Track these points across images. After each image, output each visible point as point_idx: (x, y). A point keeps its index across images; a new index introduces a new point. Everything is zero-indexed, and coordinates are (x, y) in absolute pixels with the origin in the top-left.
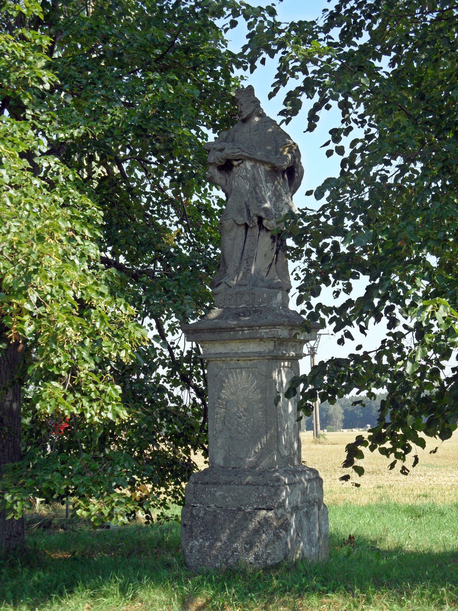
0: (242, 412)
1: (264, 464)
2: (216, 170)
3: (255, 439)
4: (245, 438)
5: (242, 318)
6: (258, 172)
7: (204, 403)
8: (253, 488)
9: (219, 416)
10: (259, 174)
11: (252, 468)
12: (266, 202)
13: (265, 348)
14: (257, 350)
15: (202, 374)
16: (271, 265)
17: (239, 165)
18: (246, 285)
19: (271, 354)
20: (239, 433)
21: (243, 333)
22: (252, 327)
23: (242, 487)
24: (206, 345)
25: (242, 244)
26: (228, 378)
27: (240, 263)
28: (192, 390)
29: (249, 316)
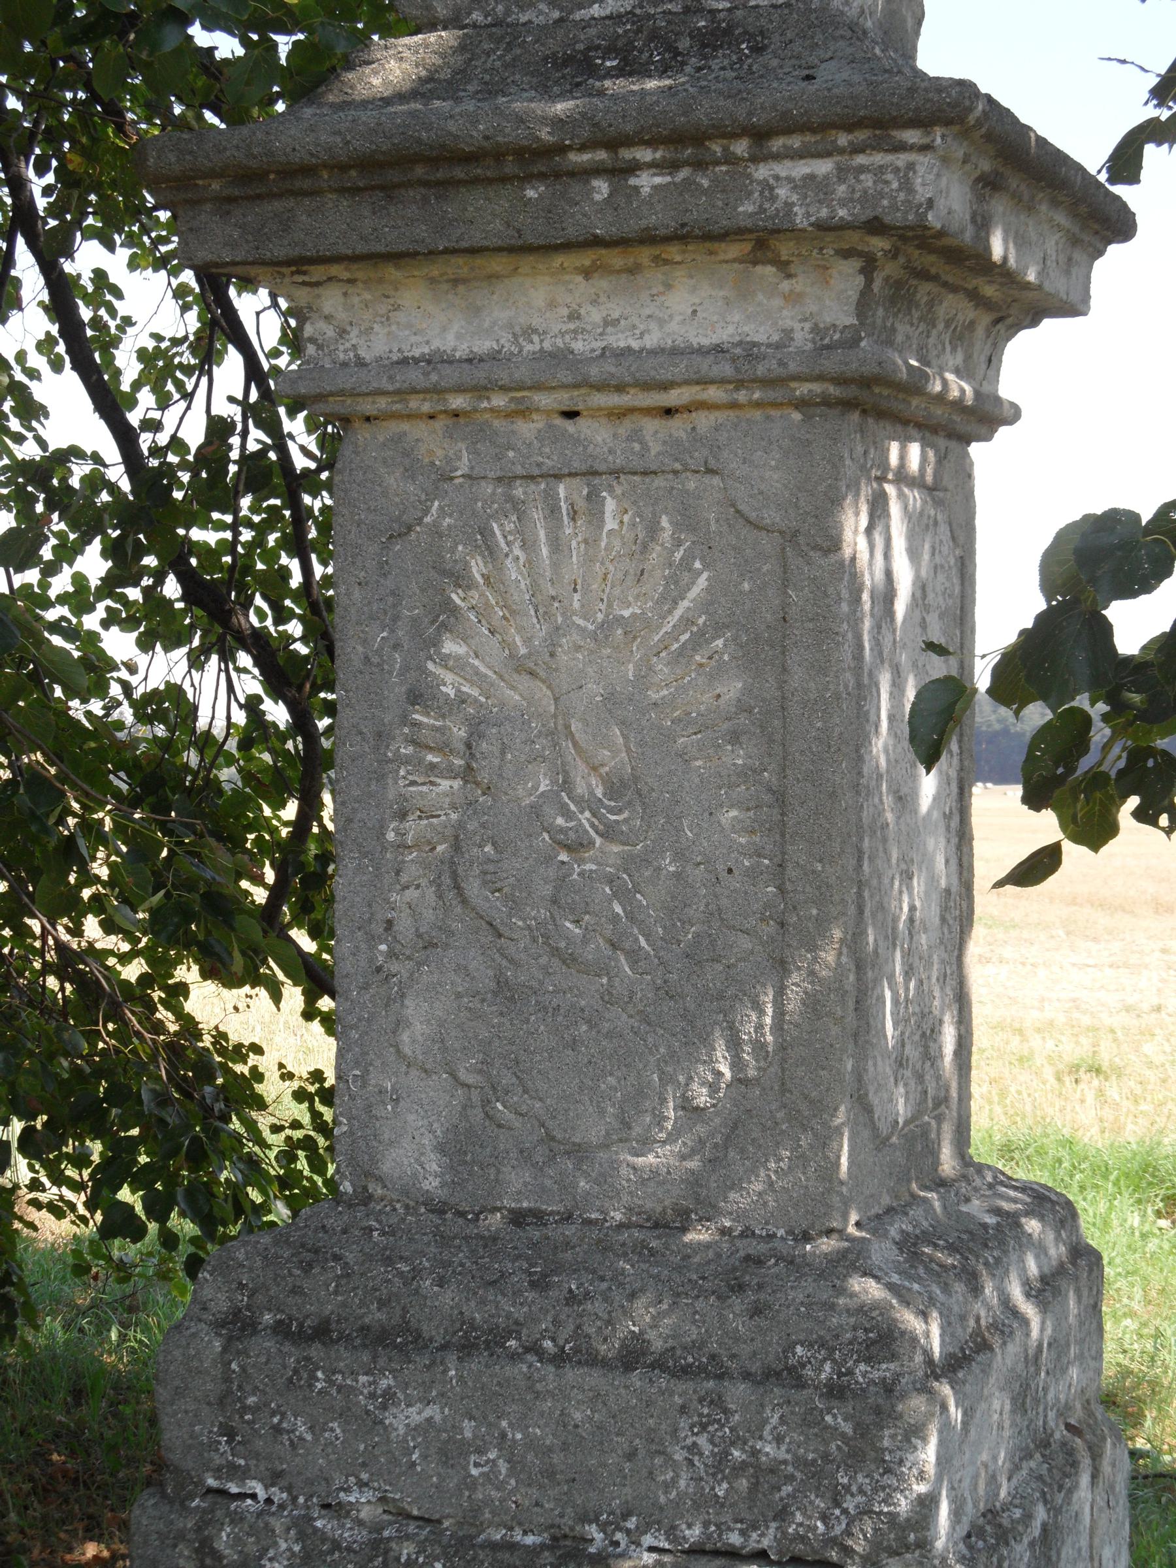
0: (591, 804)
1: (752, 1195)
3: (692, 1005)
4: (608, 998)
7: (302, 723)
8: (682, 1391)
9: (413, 827)
11: (658, 1225)
13: (788, 318)
14: (723, 334)
15: (296, 580)
19: (831, 364)
20: (570, 960)
21: (623, 194)
22: (698, 138)
23: (594, 1378)
24: (331, 300)
26: (490, 551)
28: (244, 659)
29: (663, 72)
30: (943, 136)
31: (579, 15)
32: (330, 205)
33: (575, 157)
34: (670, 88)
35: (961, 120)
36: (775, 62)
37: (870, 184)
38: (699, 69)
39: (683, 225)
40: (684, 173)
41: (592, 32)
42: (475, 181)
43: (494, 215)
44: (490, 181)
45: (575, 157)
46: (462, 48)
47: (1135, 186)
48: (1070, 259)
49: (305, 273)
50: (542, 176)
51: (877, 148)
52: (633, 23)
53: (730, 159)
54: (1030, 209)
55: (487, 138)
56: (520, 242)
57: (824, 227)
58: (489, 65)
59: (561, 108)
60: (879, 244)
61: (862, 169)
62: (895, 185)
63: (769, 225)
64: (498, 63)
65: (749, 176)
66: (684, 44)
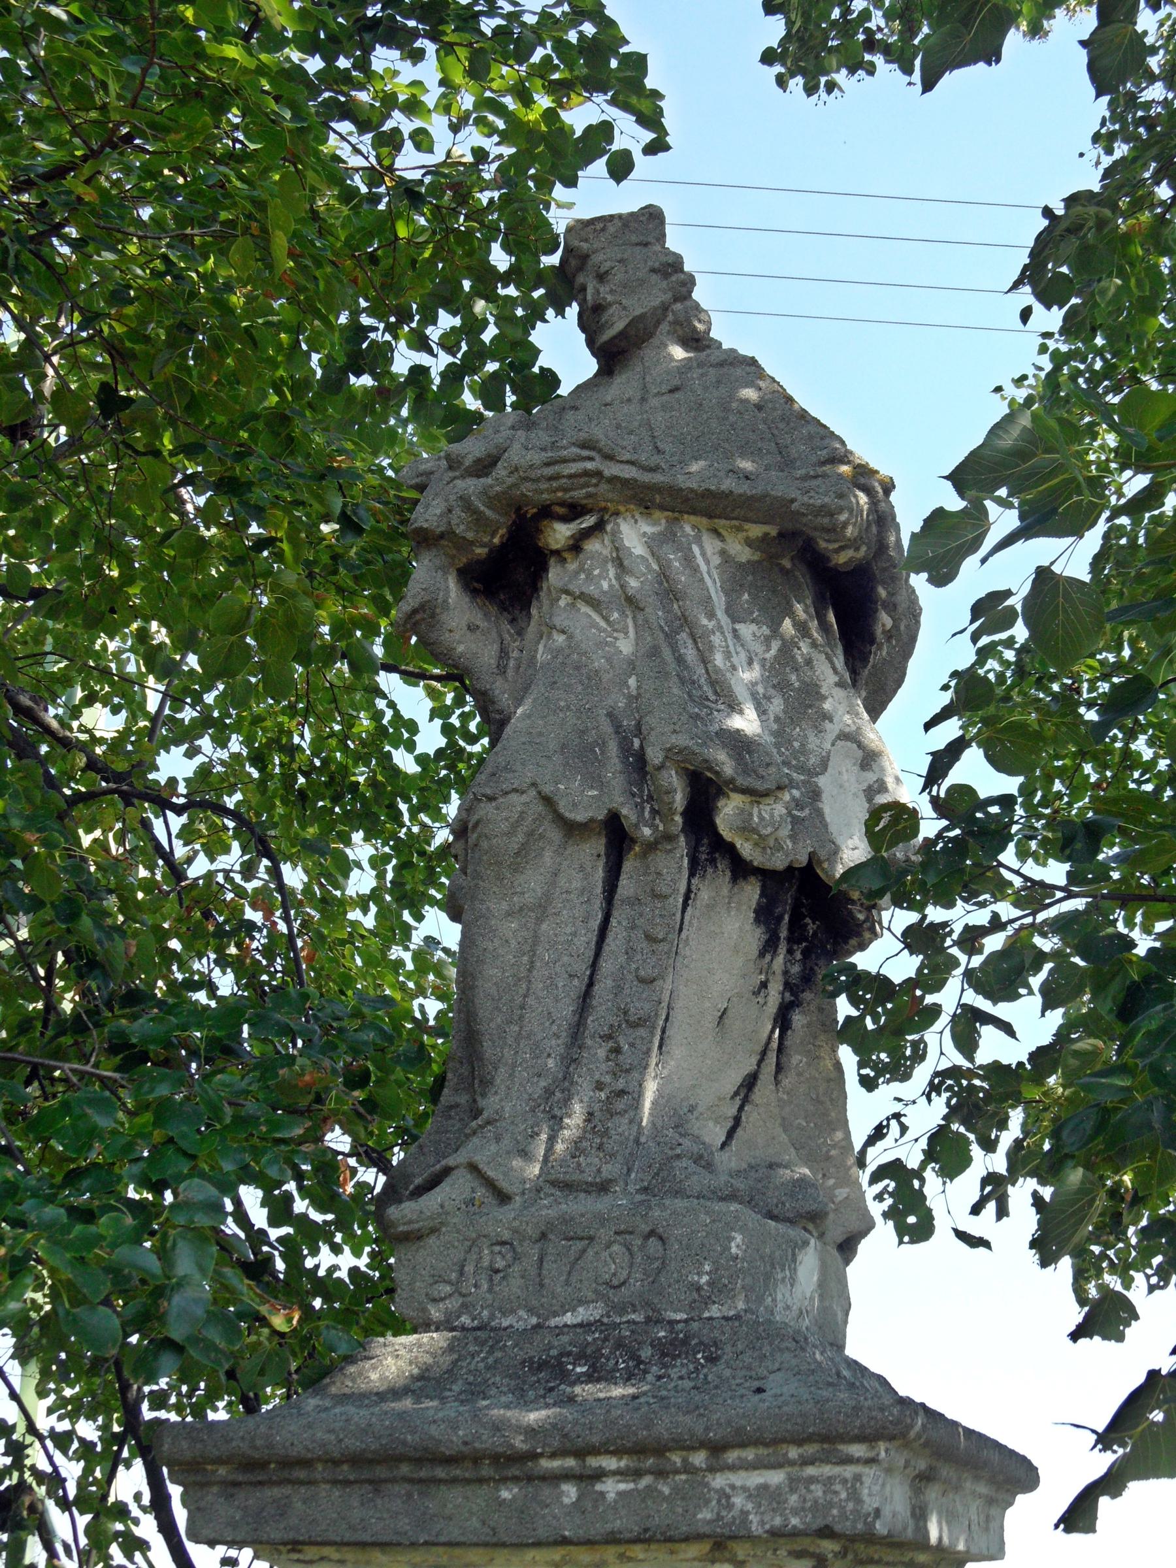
2: (452, 583)
5: (584, 1391)
6: (689, 560)
10: (696, 570)
12: (734, 707)
16: (750, 1082)
17: (576, 546)
18: (603, 1187)
22: (660, 1450)
25: (586, 939)
27: (570, 1061)
29: (628, 1378)
30: (887, 1451)
31: (553, 1322)
32: (324, 1494)
33: (546, 1464)
34: (635, 1397)
35: (904, 1435)
36: (728, 1373)
37: (820, 1493)
38: (659, 1378)
39: (646, 1530)
40: (646, 1481)
41: (565, 1339)
42: (454, 1481)
43: (471, 1513)
44: (468, 1481)
45: (546, 1464)
46: (451, 1349)
47: (1091, 1535)
48: (988, 1517)
49: (300, 1551)
50: (516, 1479)
51: (827, 1461)
52: (601, 1332)
53: (688, 1468)
54: (957, 1488)
55: (466, 1443)
56: (495, 1540)
57: (775, 1534)
58: (472, 1367)
59: (534, 1417)
60: (828, 1547)
61: (812, 1480)
62: (844, 1495)
63: (726, 1531)
64: (482, 1365)
65: (707, 1485)
66: (646, 1353)
